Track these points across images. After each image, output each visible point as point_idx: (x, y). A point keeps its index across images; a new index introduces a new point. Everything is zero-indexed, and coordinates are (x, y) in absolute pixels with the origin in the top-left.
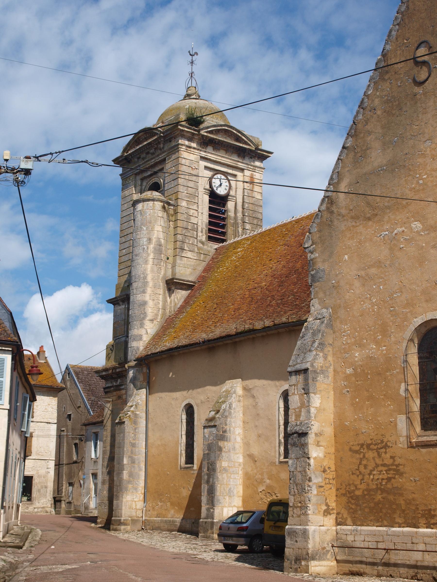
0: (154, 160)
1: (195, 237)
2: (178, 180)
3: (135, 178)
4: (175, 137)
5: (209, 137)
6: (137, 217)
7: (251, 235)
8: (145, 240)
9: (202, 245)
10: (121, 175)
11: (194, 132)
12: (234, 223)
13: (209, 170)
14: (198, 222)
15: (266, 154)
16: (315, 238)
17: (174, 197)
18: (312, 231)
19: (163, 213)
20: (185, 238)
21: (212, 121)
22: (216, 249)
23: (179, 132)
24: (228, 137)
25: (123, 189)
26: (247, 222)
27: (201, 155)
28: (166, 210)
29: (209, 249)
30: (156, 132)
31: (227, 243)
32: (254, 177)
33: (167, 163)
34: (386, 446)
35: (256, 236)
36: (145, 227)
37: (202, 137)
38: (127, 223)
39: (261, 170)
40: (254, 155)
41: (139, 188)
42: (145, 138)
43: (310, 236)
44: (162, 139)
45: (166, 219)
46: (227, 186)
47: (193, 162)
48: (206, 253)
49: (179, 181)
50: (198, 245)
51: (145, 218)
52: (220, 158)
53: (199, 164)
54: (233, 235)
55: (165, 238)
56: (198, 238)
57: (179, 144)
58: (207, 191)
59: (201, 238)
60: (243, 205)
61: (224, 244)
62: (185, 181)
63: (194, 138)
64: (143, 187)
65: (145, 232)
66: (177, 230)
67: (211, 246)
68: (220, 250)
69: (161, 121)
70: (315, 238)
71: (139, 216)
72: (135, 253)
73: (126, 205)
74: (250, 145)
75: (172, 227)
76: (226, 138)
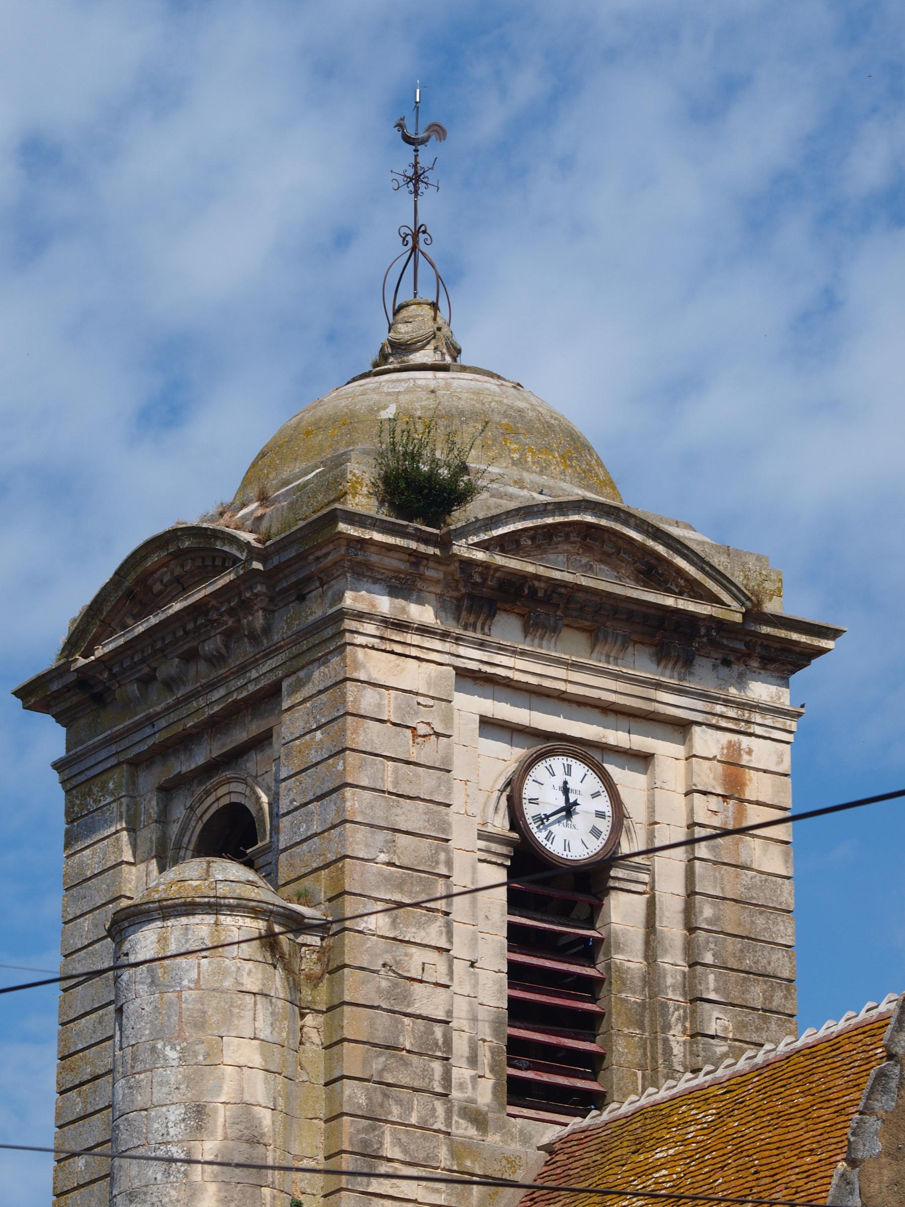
0: (222, 692)
1: (439, 1089)
2: (344, 800)
3: (133, 781)
4: (324, 578)
5: (499, 568)
6: (131, 996)
7: (720, 1072)
8: (175, 1113)
9: (472, 1132)
10: (59, 766)
11: (422, 548)
12: (643, 1005)
13: (506, 735)
14: (449, 1013)
15: (804, 639)
16: (874, 1187)
17: (321, 886)
18: (861, 1153)
19: (264, 972)
20: (386, 1096)
21: (520, 483)
22: (549, 1149)
23: (343, 550)
24: (601, 561)
25: (70, 839)
26: (713, 996)
27: (459, 663)
28: (282, 957)
29: (515, 1147)
30: (226, 548)
31: (606, 1116)
32: (745, 760)
33: (285, 706)
34: (332, 878)
35: (742, 1079)
36: (173, 1048)
37: (462, 570)
38: (93, 1016)
39: (780, 722)
40: (741, 646)
41: (149, 834)
42: (178, 580)
43: (854, 1174)
44: (259, 588)
45: (280, 1003)
46: (600, 815)
47: (421, 699)
48: (495, 1170)
49: (348, 804)
50: (454, 1130)
51: (171, 1003)
52: (560, 672)
53: (451, 711)
54: (642, 1067)
55: (280, 1101)
56: (455, 1094)
57: (342, 614)
58: (494, 847)
59: (469, 1093)
60: (689, 911)
61: (594, 1118)
62: (379, 800)
63: (421, 577)
64: (175, 829)
65: (173, 1076)
66: (340, 1059)
67: (521, 1131)
68: (571, 1155)
69: (253, 492)
70: (874, 1187)
71: (142, 989)
72: (123, 1184)
73: (86, 923)
74: (715, 600)
75: (317, 1040)
76: (588, 568)
